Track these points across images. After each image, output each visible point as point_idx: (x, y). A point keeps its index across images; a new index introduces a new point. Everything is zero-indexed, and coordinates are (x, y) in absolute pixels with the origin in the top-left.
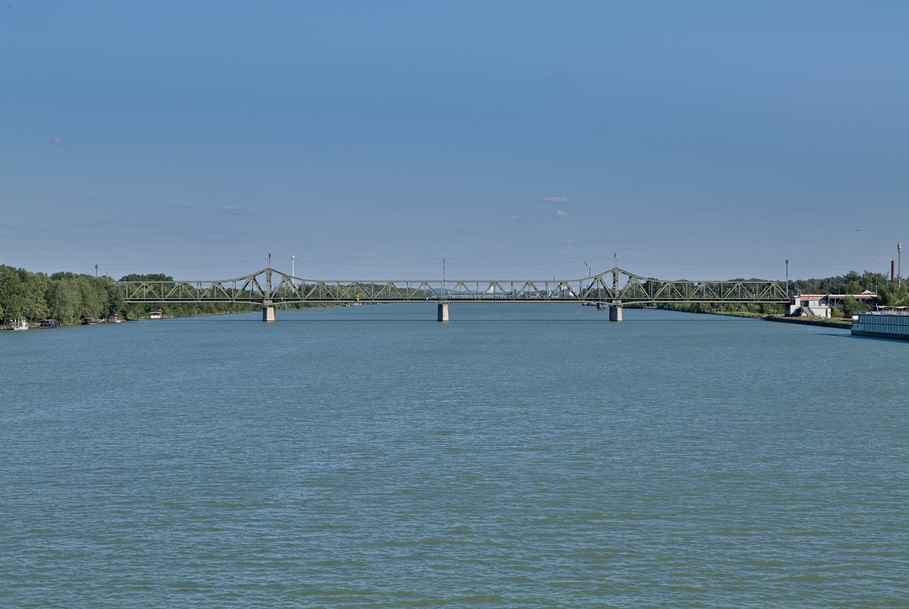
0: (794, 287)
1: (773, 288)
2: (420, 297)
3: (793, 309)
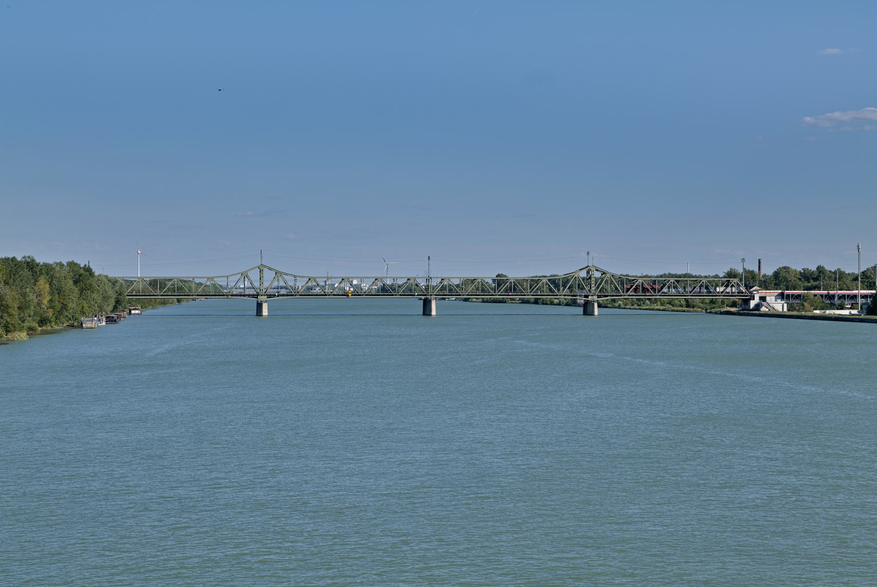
2: (409, 290)
3: (753, 304)
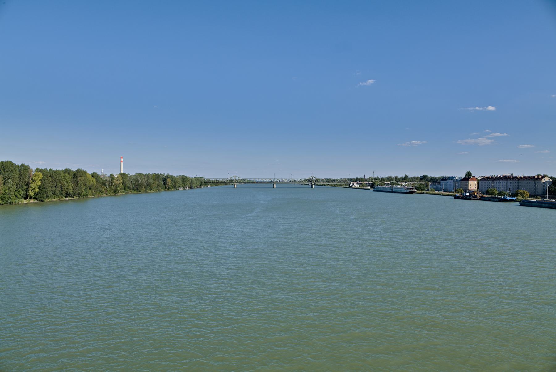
0: (352, 180)
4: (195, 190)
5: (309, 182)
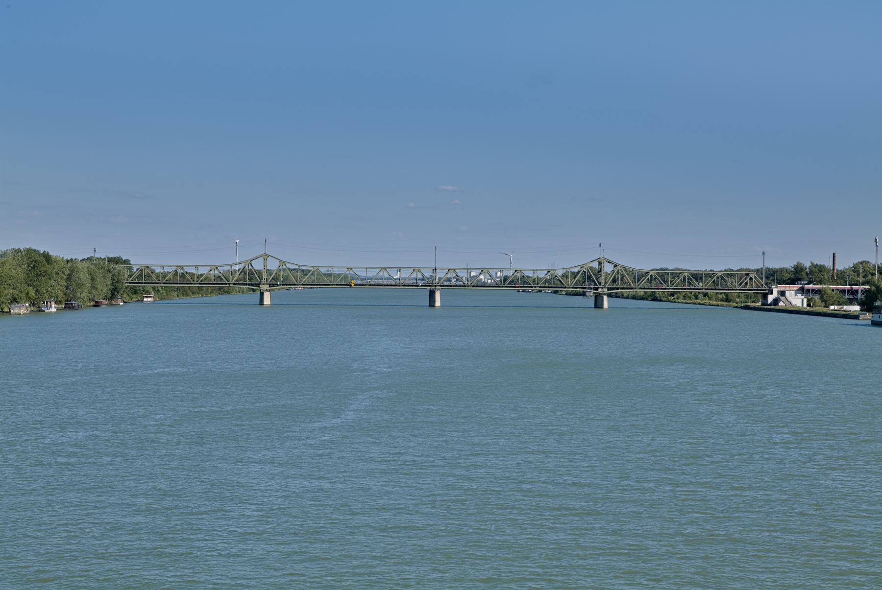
0: (774, 276)
1: (751, 279)
3: (771, 298)
4: (86, 316)
5: (586, 283)
